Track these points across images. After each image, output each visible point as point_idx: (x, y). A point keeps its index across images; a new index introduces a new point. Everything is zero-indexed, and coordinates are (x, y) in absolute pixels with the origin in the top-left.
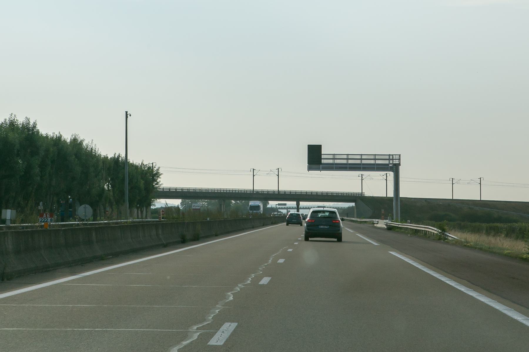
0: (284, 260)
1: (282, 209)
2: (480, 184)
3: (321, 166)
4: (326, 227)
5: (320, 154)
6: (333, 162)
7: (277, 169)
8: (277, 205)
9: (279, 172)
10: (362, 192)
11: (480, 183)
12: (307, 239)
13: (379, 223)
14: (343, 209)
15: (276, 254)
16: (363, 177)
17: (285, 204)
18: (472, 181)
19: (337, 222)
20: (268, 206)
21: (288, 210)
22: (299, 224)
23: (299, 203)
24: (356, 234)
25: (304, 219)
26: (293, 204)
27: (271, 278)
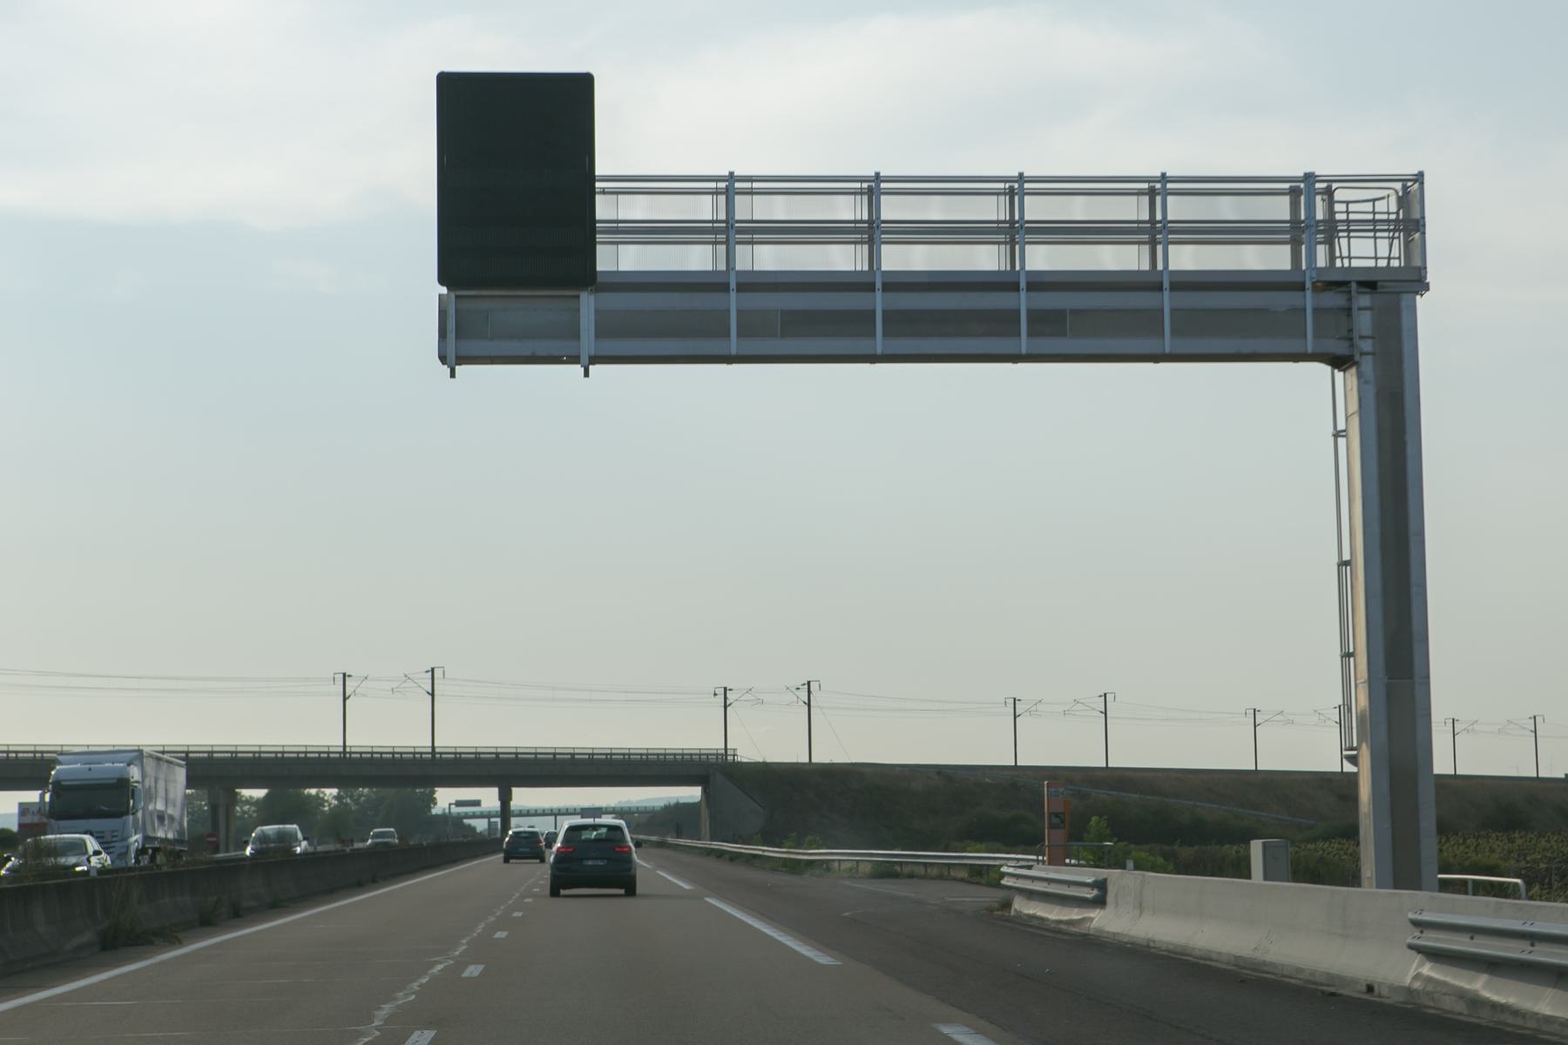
0: (481, 967)
1: (474, 816)
2: (1106, 715)
3: (588, 303)
4: (600, 863)
5: (591, 177)
6: (722, 267)
7: (427, 672)
8: (453, 806)
9: (436, 682)
10: (726, 749)
11: (1103, 710)
12: (555, 892)
13: (1110, 898)
14: (648, 812)
15: (510, 902)
16: (728, 695)
17: (477, 803)
18: (1078, 707)
19: (625, 849)
20: (434, 811)
21: (492, 820)
22: (537, 859)
23: (511, 792)
24: (707, 899)
25: (549, 845)
26: (489, 797)
27: (483, 966)
